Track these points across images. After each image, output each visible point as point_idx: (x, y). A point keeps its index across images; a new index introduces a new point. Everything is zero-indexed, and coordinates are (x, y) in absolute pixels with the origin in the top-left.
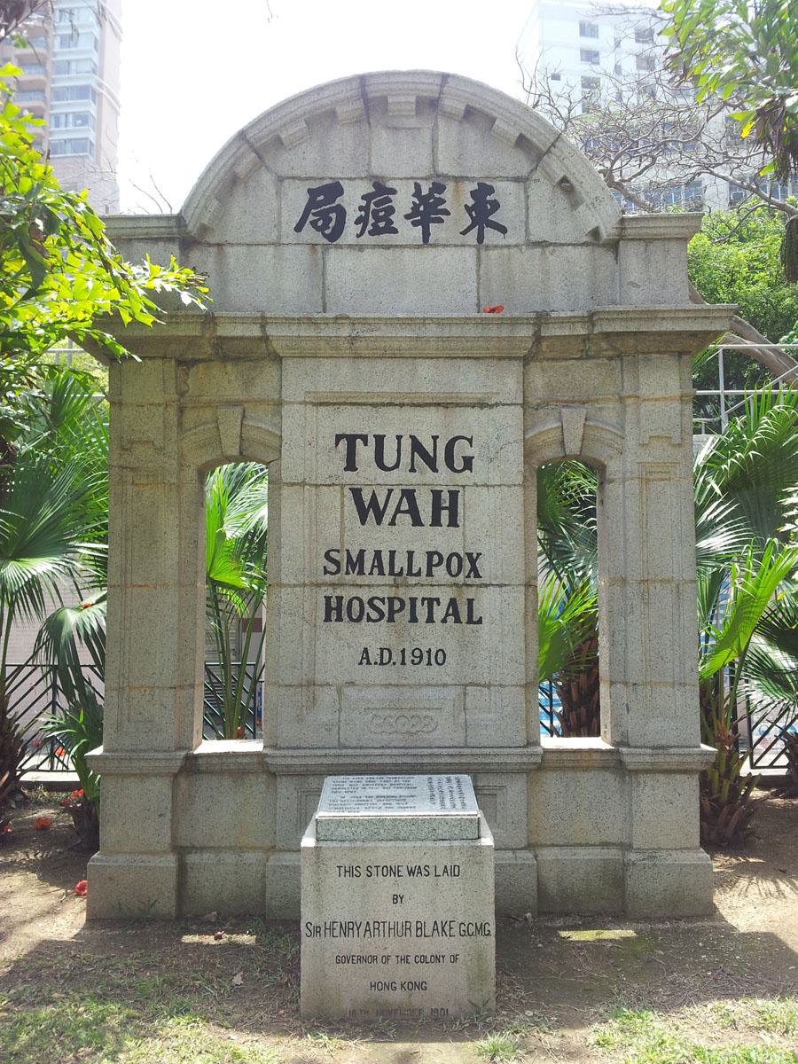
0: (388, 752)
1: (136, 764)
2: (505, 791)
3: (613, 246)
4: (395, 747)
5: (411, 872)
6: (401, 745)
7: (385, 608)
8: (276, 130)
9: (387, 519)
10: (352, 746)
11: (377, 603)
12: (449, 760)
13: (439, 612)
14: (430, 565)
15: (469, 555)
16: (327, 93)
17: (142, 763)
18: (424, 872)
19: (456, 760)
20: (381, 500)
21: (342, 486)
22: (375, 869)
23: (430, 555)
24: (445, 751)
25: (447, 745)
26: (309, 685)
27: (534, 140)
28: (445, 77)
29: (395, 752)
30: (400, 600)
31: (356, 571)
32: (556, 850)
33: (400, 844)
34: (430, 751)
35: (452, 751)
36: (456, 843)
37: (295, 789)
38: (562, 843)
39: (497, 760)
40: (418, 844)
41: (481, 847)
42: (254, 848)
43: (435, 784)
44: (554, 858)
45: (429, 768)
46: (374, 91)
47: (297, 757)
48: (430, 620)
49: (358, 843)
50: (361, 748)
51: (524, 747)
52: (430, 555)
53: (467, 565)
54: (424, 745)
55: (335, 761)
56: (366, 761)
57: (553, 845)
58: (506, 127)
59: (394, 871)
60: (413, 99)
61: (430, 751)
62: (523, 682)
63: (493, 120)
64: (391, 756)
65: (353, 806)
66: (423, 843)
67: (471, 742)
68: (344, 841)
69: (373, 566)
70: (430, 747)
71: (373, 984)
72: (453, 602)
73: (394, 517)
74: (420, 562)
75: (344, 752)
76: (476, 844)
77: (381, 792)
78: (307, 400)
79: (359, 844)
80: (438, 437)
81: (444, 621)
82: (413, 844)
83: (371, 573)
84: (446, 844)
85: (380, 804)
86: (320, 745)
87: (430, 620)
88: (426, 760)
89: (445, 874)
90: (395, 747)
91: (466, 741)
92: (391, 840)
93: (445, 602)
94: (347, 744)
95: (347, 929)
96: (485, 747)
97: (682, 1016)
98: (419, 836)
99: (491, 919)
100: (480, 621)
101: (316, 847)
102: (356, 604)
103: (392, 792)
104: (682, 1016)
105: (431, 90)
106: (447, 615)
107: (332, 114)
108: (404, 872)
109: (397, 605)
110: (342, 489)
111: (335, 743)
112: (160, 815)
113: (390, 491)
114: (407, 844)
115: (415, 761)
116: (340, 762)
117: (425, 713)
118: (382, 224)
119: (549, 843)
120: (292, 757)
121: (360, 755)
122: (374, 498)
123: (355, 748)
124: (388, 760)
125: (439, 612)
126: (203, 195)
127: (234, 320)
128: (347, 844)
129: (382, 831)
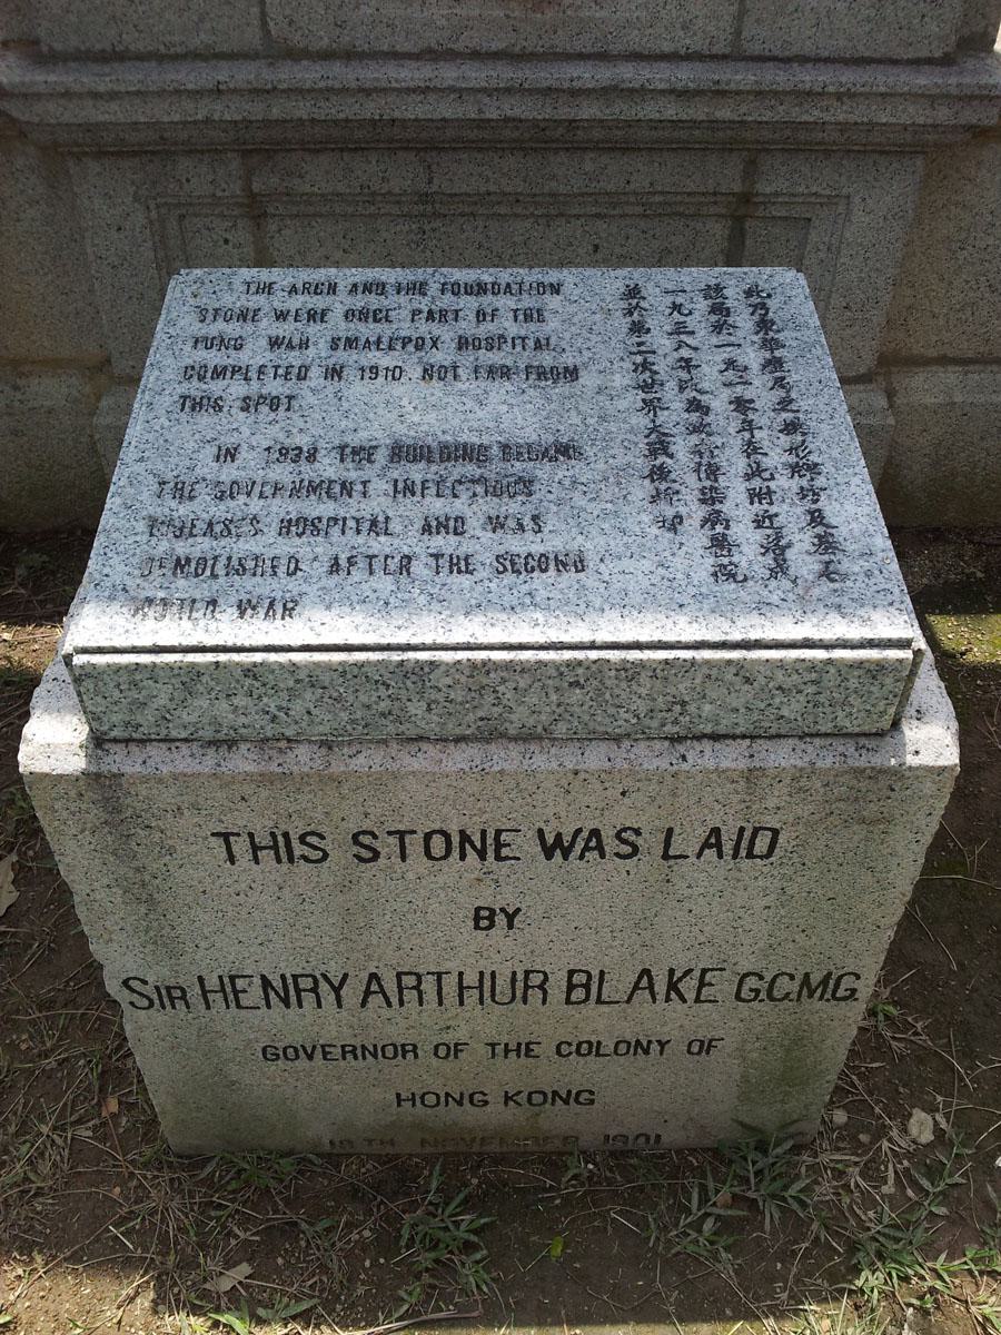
0: (449, 74)
2: (841, 209)
4: (476, 55)
5: (554, 847)
6: (495, 46)
10: (316, 46)
12: (672, 111)
18: (611, 845)
19: (698, 111)
22: (394, 840)
24: (659, 75)
25: (667, 47)
29: (477, 75)
30: (287, 1058)
32: (950, 376)
33: (505, 758)
34: (604, 74)
35: (685, 75)
36: (781, 756)
37: (136, 199)
38: (970, 354)
39: (841, 114)
40: (595, 757)
41: (901, 775)
42: (55, 365)
43: (655, 300)
44: (940, 400)
45: (597, 134)
47: (113, 96)
49: (302, 751)
50: (350, 55)
51: (947, 61)
54: (585, 44)
55: (256, 110)
56: (371, 109)
57: (944, 361)
59: (492, 846)
61: (604, 74)
64: (460, 93)
65: (270, 543)
66: (620, 755)
67: (758, 37)
68: (231, 744)
70: (603, 57)
71: (410, 1056)
75: (288, 74)
76: (877, 761)
79: (303, 758)
82: (570, 758)
84: (731, 757)
86: (198, 41)
88: (589, 111)
89: (710, 853)
90: (476, 55)
91: (738, 33)
92: (459, 740)
94: (297, 39)
95: (285, 991)
96: (803, 60)
98: (602, 723)
99: (869, 967)
101: (92, 778)
108: (527, 845)
111: (252, 37)
114: (542, 760)
115: (548, 113)
116: (275, 113)
119: (932, 353)
120: (96, 95)
121: (344, 91)
122: (559, 836)
123: (327, 56)
124: (447, 109)
128: (243, 762)
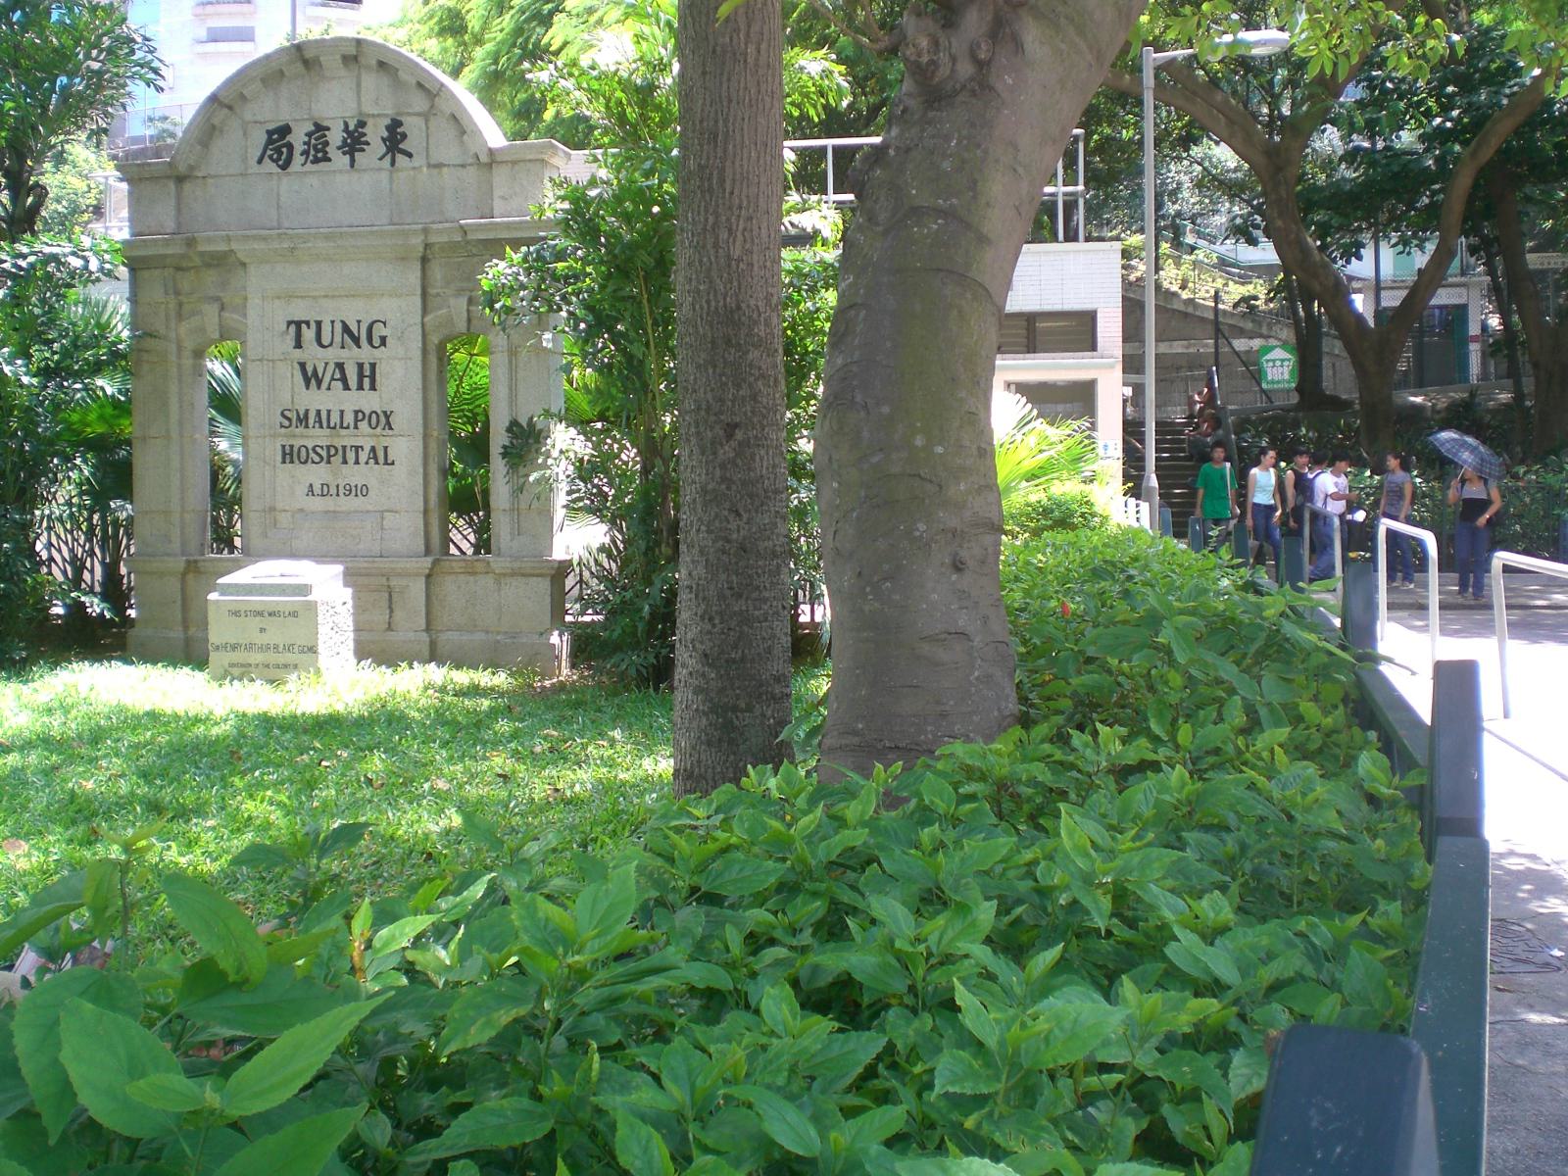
7: (324, 453)
9: (325, 385)
13: (363, 457)
14: (356, 421)
15: (385, 413)
28: (359, 42)
48: (357, 462)
52: (356, 412)
53: (383, 419)
72: (373, 449)
87: (357, 462)
93: (367, 449)
102: (303, 450)
109: (333, 452)
118: (320, 155)
125: (363, 457)
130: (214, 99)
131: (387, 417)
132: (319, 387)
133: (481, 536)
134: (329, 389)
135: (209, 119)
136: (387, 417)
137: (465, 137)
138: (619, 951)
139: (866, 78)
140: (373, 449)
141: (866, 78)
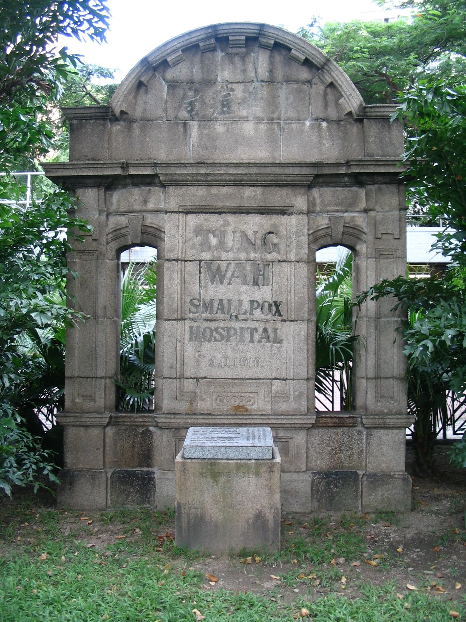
1: (83, 420)
3: (360, 121)
7: (225, 333)
8: (164, 57)
9: (226, 281)
11: (221, 330)
13: (257, 337)
14: (252, 309)
15: (275, 303)
16: (194, 35)
17: (87, 420)
20: (223, 268)
21: (200, 261)
23: (252, 302)
26: (180, 378)
27: (314, 61)
28: (262, 26)
31: (208, 312)
46: (221, 32)
48: (252, 341)
52: (252, 302)
53: (274, 308)
58: (298, 54)
60: (243, 38)
62: (306, 378)
63: (290, 49)
69: (218, 309)
72: (265, 330)
73: (231, 279)
74: (246, 306)
77: (220, 435)
78: (180, 210)
80: (257, 232)
81: (260, 341)
83: (217, 313)
85: (219, 441)
87: (252, 341)
93: (261, 330)
97: (266, 396)
100: (281, 342)
102: (208, 331)
103: (227, 435)
104: (266, 396)
105: (253, 31)
106: (262, 338)
107: (197, 46)
109: (232, 332)
110: (200, 263)
112: (97, 449)
113: (228, 264)
117: (248, 394)
118: (225, 109)
125: (257, 337)
126: (123, 94)
127: (137, 165)
129: (219, 454)
130: (145, 62)
131: (277, 306)
132: (222, 283)
133: (26, 44)
134: (229, 284)
135: (139, 77)
136: (277, 306)
137: (342, 101)
138: (211, 187)
139: (228, 333)
140: (265, 330)
141: (228, 333)
